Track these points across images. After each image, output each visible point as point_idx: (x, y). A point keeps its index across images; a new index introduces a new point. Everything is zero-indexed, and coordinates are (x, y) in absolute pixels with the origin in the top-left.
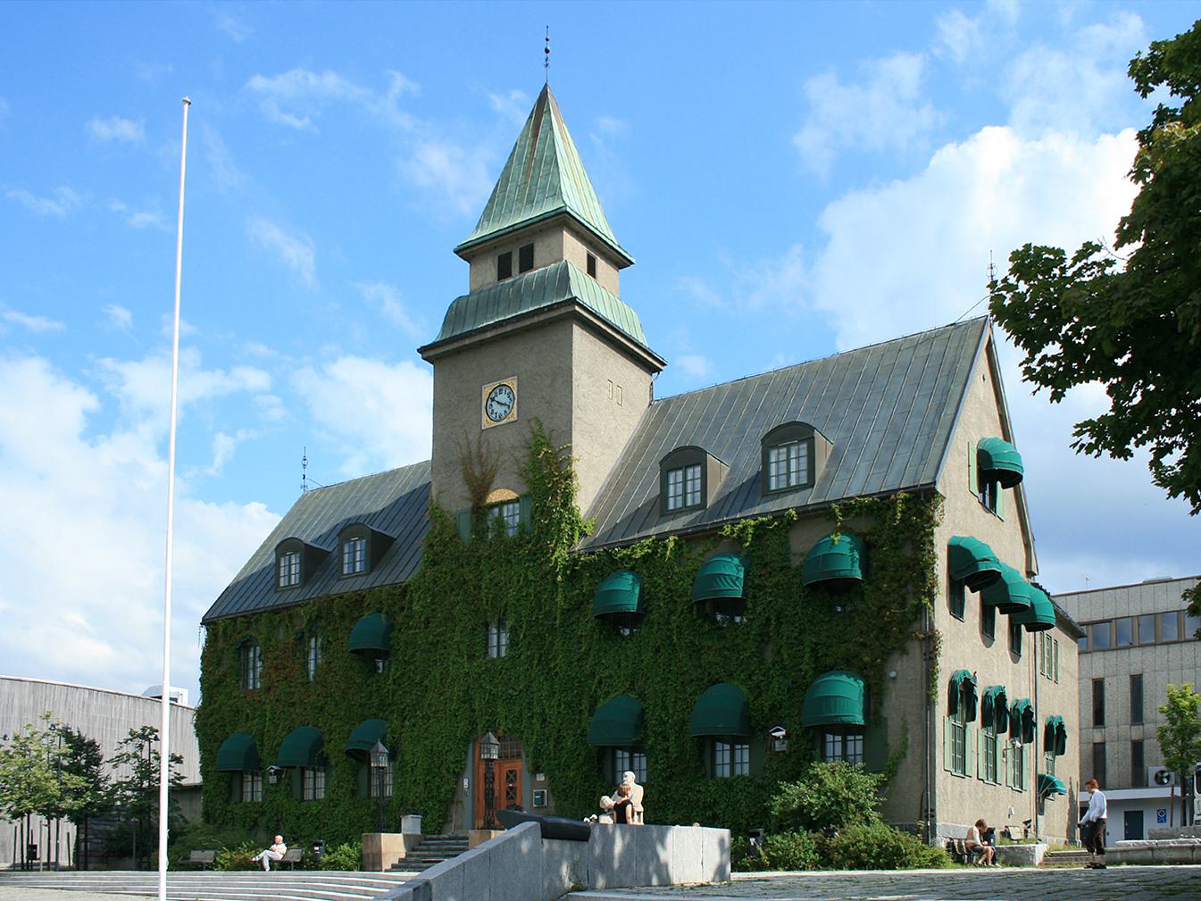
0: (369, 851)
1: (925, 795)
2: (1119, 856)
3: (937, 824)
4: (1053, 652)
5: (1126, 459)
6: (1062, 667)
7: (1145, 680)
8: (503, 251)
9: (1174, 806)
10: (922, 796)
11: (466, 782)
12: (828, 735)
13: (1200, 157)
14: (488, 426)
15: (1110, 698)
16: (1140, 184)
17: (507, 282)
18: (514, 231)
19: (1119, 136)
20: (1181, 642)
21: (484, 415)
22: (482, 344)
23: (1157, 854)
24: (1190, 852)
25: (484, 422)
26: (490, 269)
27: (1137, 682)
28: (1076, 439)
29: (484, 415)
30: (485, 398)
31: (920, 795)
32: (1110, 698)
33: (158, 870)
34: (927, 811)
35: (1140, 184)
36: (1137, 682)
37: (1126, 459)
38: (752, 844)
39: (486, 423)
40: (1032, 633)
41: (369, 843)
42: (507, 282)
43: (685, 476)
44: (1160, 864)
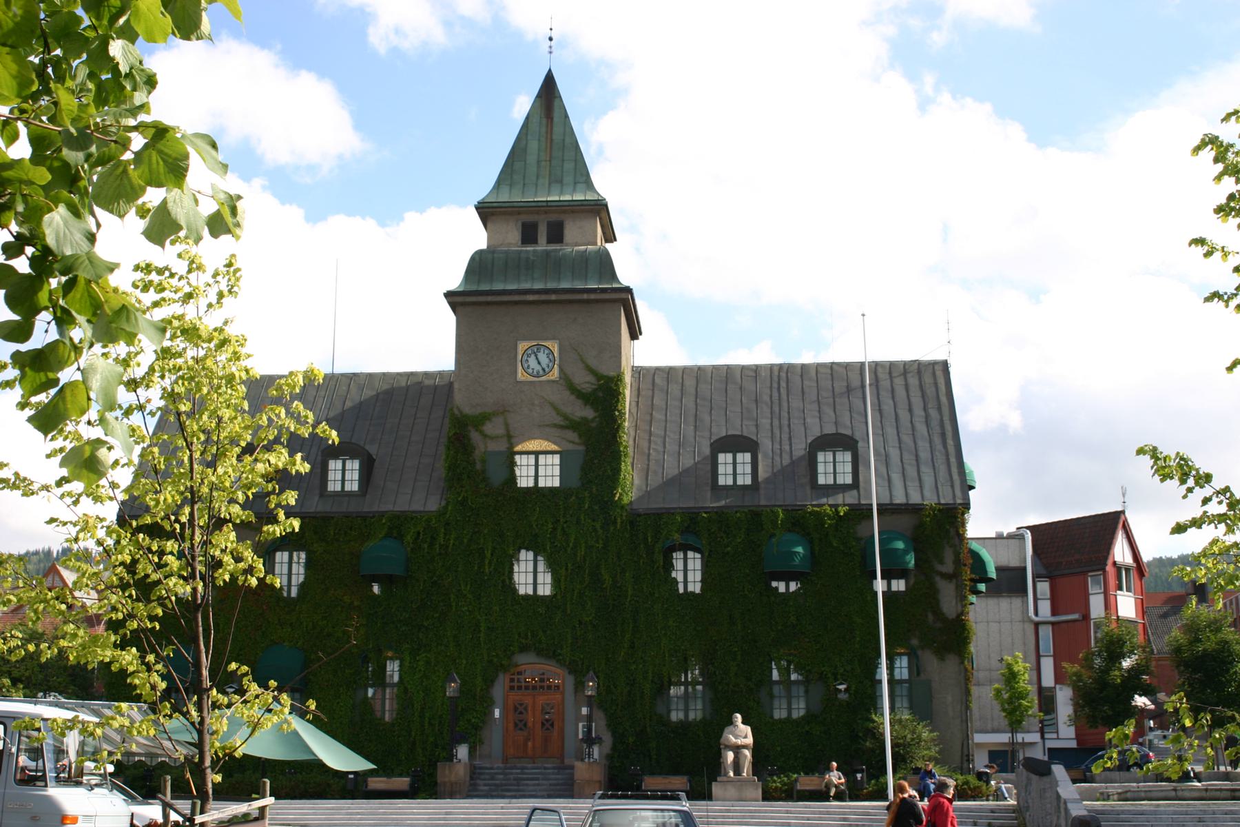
0: (447, 780)
2: (1143, 794)
10: (963, 744)
11: (497, 713)
17: (528, 249)
18: (547, 207)
19: (143, 237)
21: (520, 368)
22: (588, 302)
23: (1180, 794)
24: (1204, 792)
26: (512, 235)
28: (1185, 487)
29: (520, 368)
33: (764, 799)
38: (859, 779)
39: (521, 375)
41: (447, 772)
42: (528, 249)
44: (974, 798)
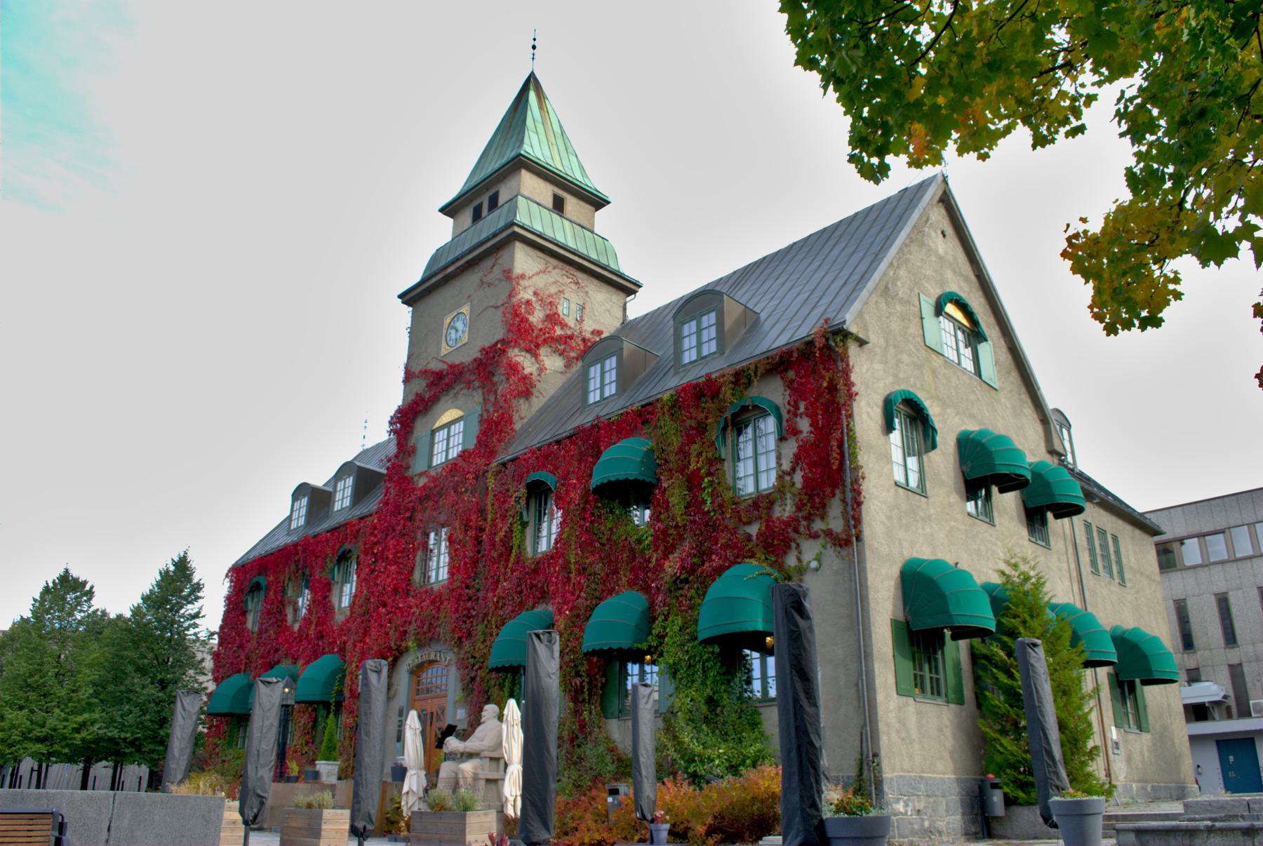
1: (864, 731)
3: (885, 776)
4: (1112, 549)
5: (1178, 296)
6: (1131, 568)
7: (1232, 599)
8: (476, 203)
9: (1088, 812)
12: (630, 665)
13: (2, 706)
14: (446, 353)
15: (1238, 613)
16: (195, 581)
20: (1207, 566)
25: (443, 350)
27: (1223, 603)
30: (446, 326)
31: (859, 734)
32: (1238, 613)
34: (868, 757)
35: (195, 581)
36: (1223, 603)
37: (1178, 296)
40: (1066, 520)
43: (699, 325)
